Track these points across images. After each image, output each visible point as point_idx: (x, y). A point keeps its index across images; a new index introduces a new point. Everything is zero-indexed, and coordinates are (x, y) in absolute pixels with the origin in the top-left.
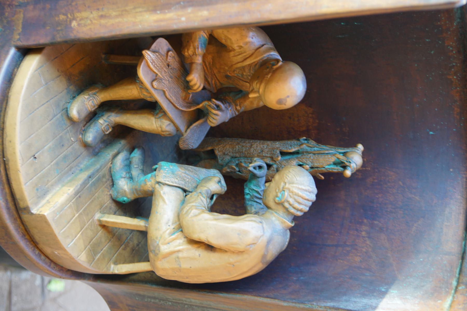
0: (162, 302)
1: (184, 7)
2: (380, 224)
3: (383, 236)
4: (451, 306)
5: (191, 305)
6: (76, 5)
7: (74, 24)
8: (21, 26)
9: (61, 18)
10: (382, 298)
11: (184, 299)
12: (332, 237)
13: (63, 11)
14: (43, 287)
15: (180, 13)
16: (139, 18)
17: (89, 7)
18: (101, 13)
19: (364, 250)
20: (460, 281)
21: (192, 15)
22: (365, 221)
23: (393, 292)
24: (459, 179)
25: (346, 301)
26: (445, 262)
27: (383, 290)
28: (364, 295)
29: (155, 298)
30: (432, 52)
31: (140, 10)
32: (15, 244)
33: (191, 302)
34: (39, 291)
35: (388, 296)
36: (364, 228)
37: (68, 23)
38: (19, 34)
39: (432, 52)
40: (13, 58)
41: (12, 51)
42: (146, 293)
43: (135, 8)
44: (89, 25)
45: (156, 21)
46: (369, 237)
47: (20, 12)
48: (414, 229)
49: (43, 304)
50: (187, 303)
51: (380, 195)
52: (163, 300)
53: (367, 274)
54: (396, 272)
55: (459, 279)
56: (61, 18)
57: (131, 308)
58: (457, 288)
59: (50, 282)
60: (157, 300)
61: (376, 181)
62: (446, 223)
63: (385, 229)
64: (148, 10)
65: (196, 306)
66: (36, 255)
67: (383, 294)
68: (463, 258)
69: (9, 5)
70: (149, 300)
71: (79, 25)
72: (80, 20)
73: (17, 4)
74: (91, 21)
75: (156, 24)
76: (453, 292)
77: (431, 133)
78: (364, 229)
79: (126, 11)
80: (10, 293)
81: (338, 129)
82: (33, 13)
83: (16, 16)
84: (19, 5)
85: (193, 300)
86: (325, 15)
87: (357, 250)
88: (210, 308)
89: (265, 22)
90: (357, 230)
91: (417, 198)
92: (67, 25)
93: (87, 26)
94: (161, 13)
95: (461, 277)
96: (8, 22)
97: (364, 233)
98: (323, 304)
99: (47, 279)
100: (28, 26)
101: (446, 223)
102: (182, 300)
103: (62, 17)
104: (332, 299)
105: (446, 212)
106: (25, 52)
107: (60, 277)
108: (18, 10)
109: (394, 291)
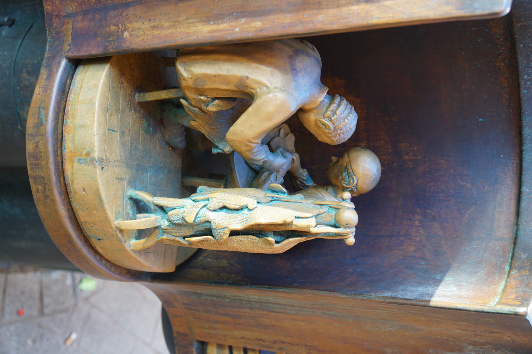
0: (219, 299)
1: (237, 18)
2: (433, 213)
3: (436, 225)
4: (504, 290)
5: (249, 301)
6: (127, 15)
7: (126, 34)
8: (70, 37)
9: (112, 29)
10: (438, 286)
11: (242, 295)
12: (386, 227)
13: (114, 21)
14: (75, 286)
15: (233, 24)
16: (192, 29)
17: (140, 18)
18: (153, 24)
19: (418, 239)
20: (513, 266)
21: (245, 26)
22: (418, 210)
23: (448, 279)
24: (510, 165)
25: (403, 290)
26: (498, 248)
27: (438, 278)
28: (420, 284)
29: (212, 296)
30: (480, 40)
31: (193, 20)
32: (77, 250)
33: (249, 298)
34: (70, 291)
35: (443, 283)
36: (417, 217)
37: (120, 33)
38: (69, 45)
39: (480, 40)
40: (65, 69)
41: (64, 62)
42: (204, 292)
43: (187, 19)
44: (142, 35)
45: (210, 32)
46: (422, 227)
47: (69, 22)
48: (466, 216)
49: (76, 305)
50: (246, 299)
51: (432, 184)
52: (221, 297)
53: (422, 263)
54: (450, 260)
55: (511, 263)
56: (112, 29)
57: (187, 306)
58: (509, 272)
59: (81, 281)
60: (215, 298)
61: (427, 170)
62: (498, 210)
63: (437, 218)
64: (200, 21)
65: (254, 302)
66: (98, 260)
67: (438, 282)
68: (515, 243)
69: (57, 16)
70: (207, 297)
71: (131, 35)
72: (132, 31)
73: (65, 14)
74: (143, 31)
75: (210, 35)
76: (506, 276)
77: (481, 120)
78: (417, 218)
79: (178, 21)
80: (41, 295)
81: (387, 119)
82: (82, 24)
83: (64, 27)
84: (67, 16)
85: (251, 296)
86: (377, 25)
87: (411, 239)
88: (269, 303)
89: (318, 32)
90: (410, 219)
91: (469, 185)
92: (119, 37)
93: (139, 37)
94: (214, 24)
95: (513, 262)
96: (57, 33)
97: (417, 223)
98: (381, 295)
99: (78, 275)
100: (79, 37)
101: (498, 210)
102: (241, 297)
103: (113, 28)
104: (389, 289)
105: (498, 199)
106: (76, 63)
107: (120, 280)
108: (67, 20)
109: (449, 279)
